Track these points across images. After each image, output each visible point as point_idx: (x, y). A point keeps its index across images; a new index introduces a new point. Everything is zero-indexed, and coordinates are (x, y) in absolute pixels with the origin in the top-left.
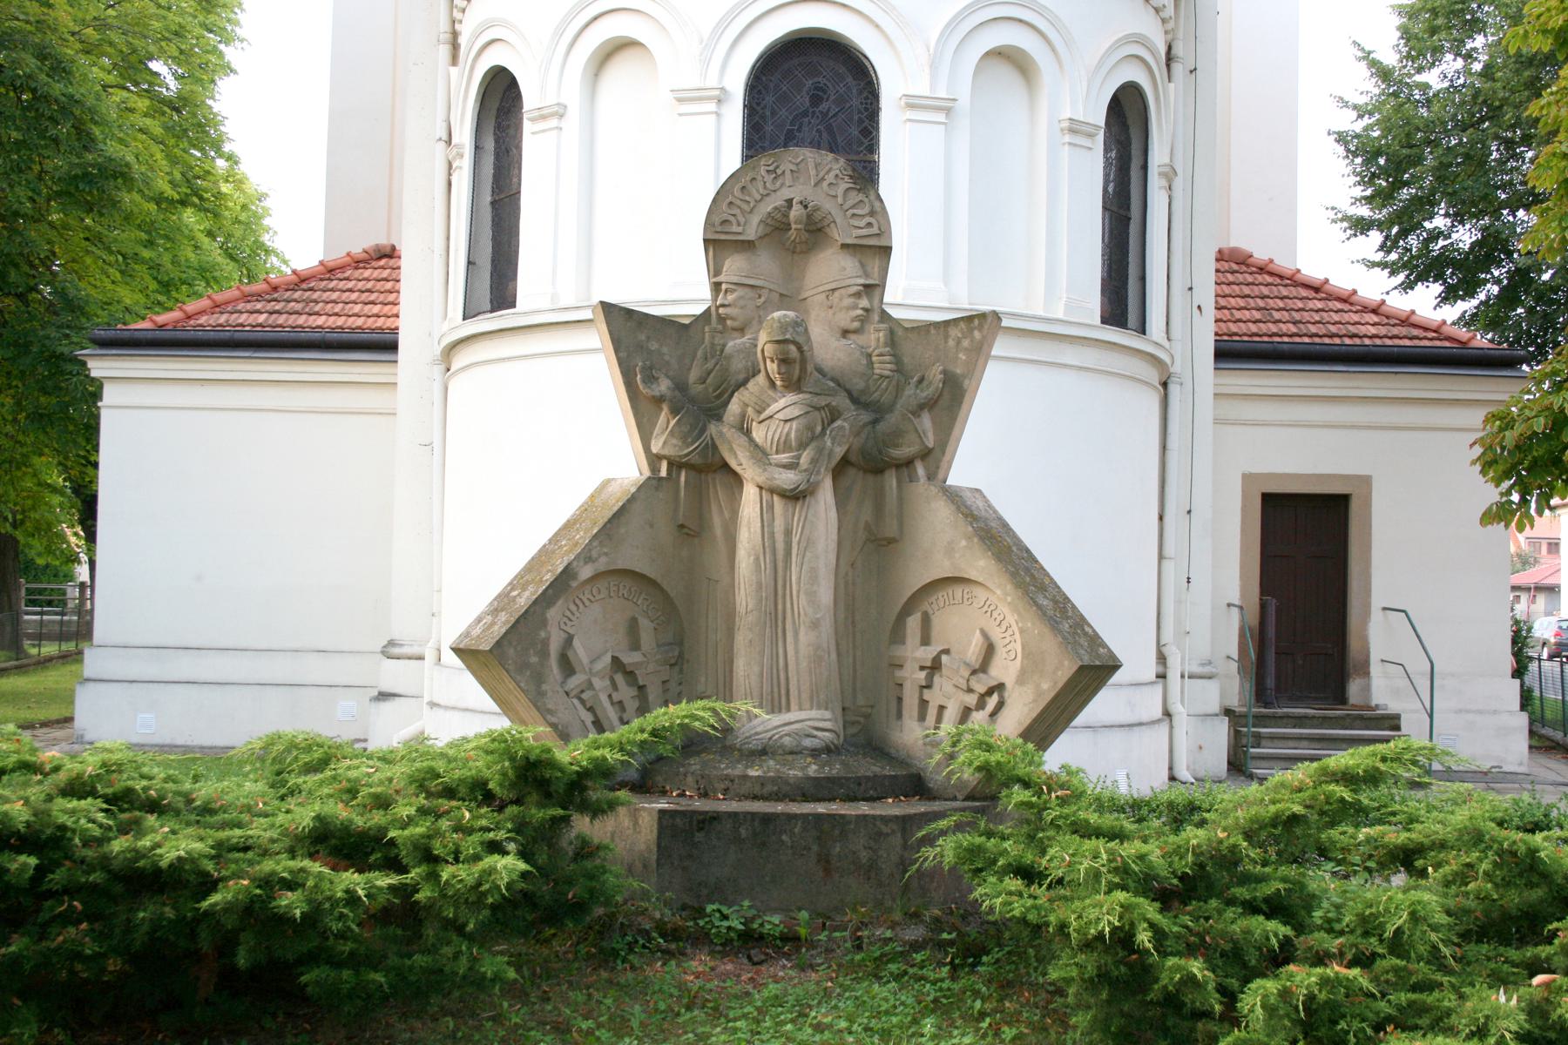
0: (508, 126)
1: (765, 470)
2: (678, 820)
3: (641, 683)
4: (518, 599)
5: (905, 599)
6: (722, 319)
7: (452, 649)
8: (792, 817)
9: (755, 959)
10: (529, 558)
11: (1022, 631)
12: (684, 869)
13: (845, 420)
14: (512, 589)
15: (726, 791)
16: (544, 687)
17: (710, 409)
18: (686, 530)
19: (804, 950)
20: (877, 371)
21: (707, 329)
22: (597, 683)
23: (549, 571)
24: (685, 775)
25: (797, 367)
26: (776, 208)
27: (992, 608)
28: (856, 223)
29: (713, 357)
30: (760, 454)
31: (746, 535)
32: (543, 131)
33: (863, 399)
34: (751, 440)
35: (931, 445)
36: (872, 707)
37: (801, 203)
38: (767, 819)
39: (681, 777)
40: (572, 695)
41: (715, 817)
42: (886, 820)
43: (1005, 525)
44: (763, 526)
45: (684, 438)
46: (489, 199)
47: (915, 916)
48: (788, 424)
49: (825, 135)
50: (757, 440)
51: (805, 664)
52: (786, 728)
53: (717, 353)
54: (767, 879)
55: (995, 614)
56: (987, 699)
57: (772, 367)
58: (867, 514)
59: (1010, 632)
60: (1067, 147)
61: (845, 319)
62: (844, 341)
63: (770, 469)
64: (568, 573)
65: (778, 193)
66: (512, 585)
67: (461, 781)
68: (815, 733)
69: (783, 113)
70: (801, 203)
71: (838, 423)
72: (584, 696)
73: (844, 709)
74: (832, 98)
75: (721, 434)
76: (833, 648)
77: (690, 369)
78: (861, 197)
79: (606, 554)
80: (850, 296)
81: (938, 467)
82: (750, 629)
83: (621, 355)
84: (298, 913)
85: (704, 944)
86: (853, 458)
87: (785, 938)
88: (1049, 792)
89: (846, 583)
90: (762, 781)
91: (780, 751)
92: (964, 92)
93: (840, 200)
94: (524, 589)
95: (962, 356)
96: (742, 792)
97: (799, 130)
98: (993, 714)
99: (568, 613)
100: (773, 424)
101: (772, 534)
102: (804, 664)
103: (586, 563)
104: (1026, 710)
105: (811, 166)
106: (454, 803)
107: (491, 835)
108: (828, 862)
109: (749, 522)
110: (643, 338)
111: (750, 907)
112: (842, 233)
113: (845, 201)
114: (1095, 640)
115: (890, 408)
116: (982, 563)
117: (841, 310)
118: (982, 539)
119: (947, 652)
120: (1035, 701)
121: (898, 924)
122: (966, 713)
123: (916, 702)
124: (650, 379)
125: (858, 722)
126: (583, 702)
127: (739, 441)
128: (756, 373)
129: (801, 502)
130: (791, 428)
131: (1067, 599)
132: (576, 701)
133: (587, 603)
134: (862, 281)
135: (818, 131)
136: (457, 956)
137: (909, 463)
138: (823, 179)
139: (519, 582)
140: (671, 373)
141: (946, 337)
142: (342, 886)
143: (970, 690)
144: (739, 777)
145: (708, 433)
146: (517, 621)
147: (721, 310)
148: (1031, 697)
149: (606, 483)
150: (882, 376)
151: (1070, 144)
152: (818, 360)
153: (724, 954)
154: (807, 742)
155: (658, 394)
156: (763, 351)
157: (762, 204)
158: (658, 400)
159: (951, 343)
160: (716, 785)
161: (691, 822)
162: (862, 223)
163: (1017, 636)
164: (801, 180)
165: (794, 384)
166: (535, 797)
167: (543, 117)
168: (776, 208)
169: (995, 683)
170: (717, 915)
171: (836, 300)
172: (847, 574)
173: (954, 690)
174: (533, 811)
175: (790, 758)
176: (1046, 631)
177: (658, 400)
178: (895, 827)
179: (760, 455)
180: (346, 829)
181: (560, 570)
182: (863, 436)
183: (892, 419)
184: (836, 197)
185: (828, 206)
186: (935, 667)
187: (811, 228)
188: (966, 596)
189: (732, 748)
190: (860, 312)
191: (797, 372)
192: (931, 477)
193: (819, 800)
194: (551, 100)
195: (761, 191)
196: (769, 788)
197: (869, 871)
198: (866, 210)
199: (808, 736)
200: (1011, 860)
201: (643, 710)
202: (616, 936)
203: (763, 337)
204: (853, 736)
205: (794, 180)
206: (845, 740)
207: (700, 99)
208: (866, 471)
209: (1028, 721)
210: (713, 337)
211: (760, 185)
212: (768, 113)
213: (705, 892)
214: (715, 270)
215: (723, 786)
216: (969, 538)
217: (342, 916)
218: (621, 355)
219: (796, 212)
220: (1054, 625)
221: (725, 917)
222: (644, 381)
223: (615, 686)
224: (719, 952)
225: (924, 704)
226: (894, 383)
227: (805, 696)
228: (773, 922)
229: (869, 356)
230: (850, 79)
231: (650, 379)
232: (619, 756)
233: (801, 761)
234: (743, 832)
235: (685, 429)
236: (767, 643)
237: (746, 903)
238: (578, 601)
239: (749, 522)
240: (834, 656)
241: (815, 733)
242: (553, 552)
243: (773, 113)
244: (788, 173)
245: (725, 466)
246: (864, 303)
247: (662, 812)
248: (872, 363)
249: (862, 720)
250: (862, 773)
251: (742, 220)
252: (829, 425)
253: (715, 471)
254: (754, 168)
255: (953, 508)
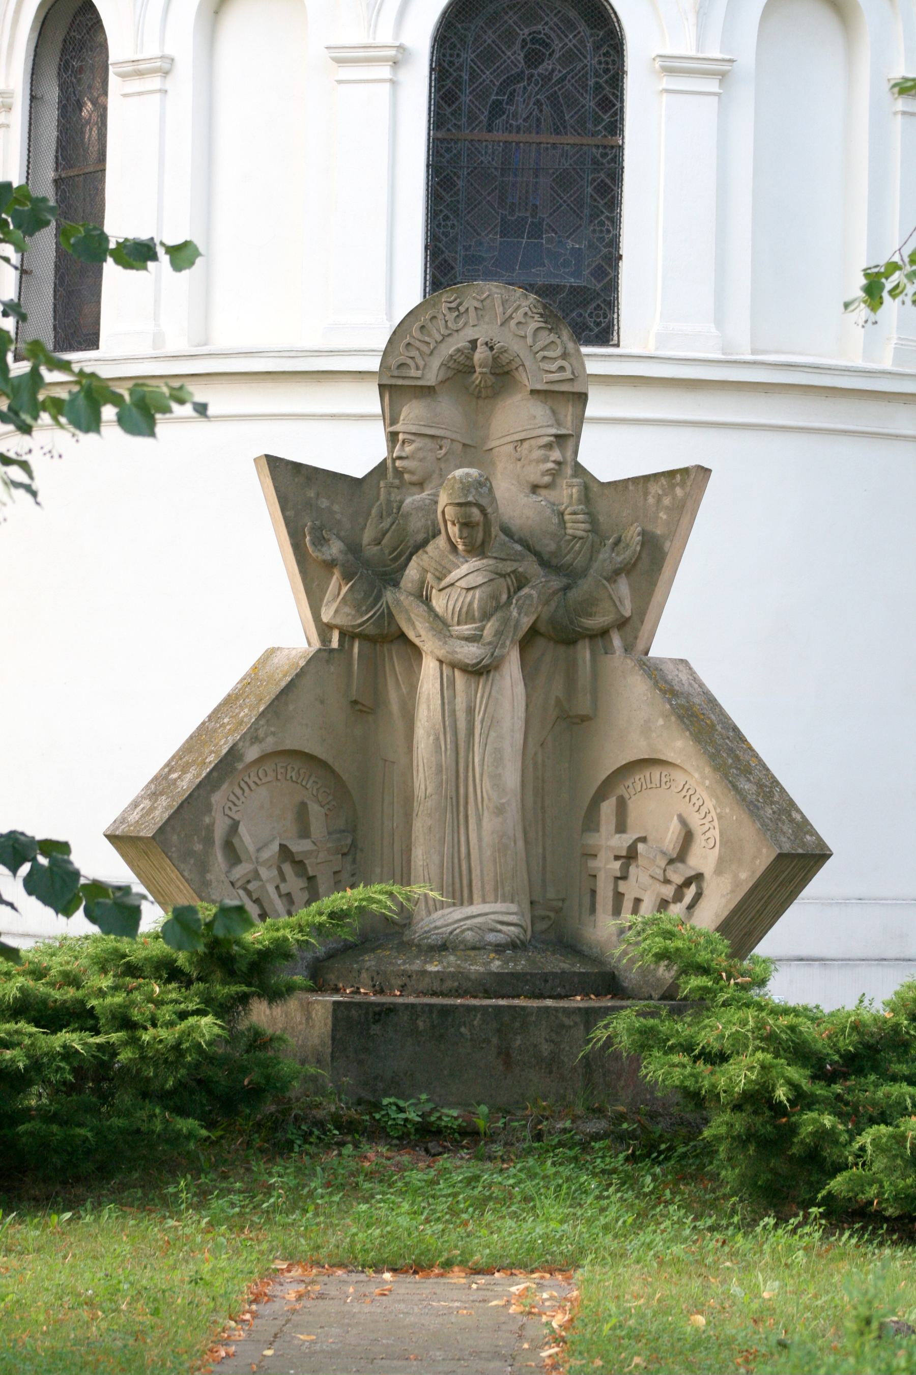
0: (81, 70)
1: (445, 643)
2: (353, 1012)
3: (311, 874)
4: (179, 783)
5: (600, 782)
6: (399, 473)
7: (107, 836)
8: (470, 1009)
9: (433, 1151)
10: (187, 736)
11: (720, 817)
12: (361, 1062)
13: (533, 587)
14: (170, 772)
15: (403, 988)
16: (209, 876)
17: (385, 573)
18: (359, 707)
19: (482, 1143)
20: (569, 531)
21: (382, 484)
22: (264, 873)
23: (211, 752)
24: (359, 972)
25: (481, 528)
26: (458, 350)
27: (691, 792)
28: (546, 366)
29: (389, 515)
30: (440, 624)
31: (426, 713)
32: (140, 94)
33: (554, 562)
34: (431, 609)
35: (627, 613)
36: (563, 900)
37: (486, 344)
38: (445, 1011)
39: (355, 974)
40: (238, 884)
41: (391, 1010)
42: (567, 1011)
43: (712, 701)
44: (443, 704)
45: (357, 607)
46: (51, 175)
47: (599, 1112)
48: (471, 593)
49: (547, 109)
50: (438, 609)
51: (489, 853)
52: (469, 922)
53: (394, 511)
54: (445, 1072)
55: (694, 799)
56: (685, 890)
57: (454, 530)
58: (558, 689)
59: (709, 818)
60: (899, 117)
61: (535, 473)
62: (534, 498)
63: (451, 641)
64: (233, 754)
65: (462, 333)
66: (170, 766)
67: (147, 959)
68: (499, 927)
69: (487, 75)
70: (486, 344)
71: (525, 591)
72: (250, 887)
73: (532, 903)
74: (557, 55)
75: (398, 602)
76: (520, 835)
77: (363, 528)
78: (552, 337)
79: (273, 734)
80: (540, 447)
81: (636, 638)
82: (430, 815)
83: (288, 513)
84: (21, 1065)
85: (380, 1138)
86: (542, 628)
87: (463, 1133)
88: (729, 979)
89: (535, 764)
90: (441, 977)
91: (462, 947)
92: (746, 57)
93: (529, 341)
94: (185, 770)
95: (663, 515)
96: (421, 988)
97: (510, 101)
98: (691, 907)
99: (233, 798)
100: (455, 593)
101: (453, 712)
102: (488, 853)
103: (252, 743)
104: (724, 901)
105: (498, 303)
106: (141, 981)
107: (182, 1006)
108: (508, 1055)
109: (428, 700)
110: (312, 495)
111: (428, 1100)
112: (529, 379)
113: (534, 342)
114: (804, 827)
115: (584, 573)
116: (679, 744)
117: (531, 461)
118: (680, 718)
119: (643, 840)
120: (732, 891)
121: (580, 1117)
122: (663, 904)
123: (610, 894)
124: (320, 541)
125: (549, 917)
126: (249, 893)
127: (417, 611)
128: (436, 534)
129: (484, 676)
130: (473, 597)
131: (775, 782)
132: (241, 892)
133: (253, 786)
134: (554, 431)
135: (538, 103)
136: (152, 1116)
137: (604, 633)
138: (511, 317)
139: (179, 762)
140: (343, 534)
141: (646, 494)
142: (60, 1042)
143: (667, 881)
144: (417, 972)
145: (383, 600)
146: (181, 806)
147: (398, 463)
148: (729, 887)
149: (271, 653)
150: (574, 537)
151: (904, 113)
152: (505, 519)
153: (400, 1148)
154: (491, 937)
155: (329, 558)
156: (443, 512)
157: (443, 345)
158: (330, 565)
159: (651, 500)
160: (393, 981)
161: (367, 1013)
162: (554, 367)
163: (716, 823)
164: (487, 319)
165: (477, 549)
166: (219, 974)
167: (140, 74)
168: (458, 350)
169: (693, 873)
170: (394, 1108)
171: (525, 452)
172: (536, 754)
173: (651, 881)
174: (218, 987)
175: (472, 953)
176: (745, 818)
177: (330, 565)
178: (578, 1019)
179: (441, 626)
180: (44, 1001)
181: (224, 751)
182: (553, 604)
183: (585, 586)
184: (525, 337)
185: (516, 347)
186: (631, 856)
187: (497, 371)
188: (664, 780)
189: (409, 945)
190: (550, 465)
191: (480, 536)
192: (628, 649)
193: (503, 997)
194: (151, 50)
195: (443, 331)
196: (450, 984)
197: (552, 1064)
198: (559, 352)
199: (492, 930)
200: (681, 1040)
201: (314, 896)
202: (291, 1128)
203: (443, 499)
204: (543, 932)
205: (479, 318)
206: (533, 936)
207: (368, 60)
208: (557, 642)
209: (726, 913)
210: (390, 494)
211: (441, 323)
212: (466, 77)
213: (381, 1085)
214: (391, 417)
215: (400, 983)
216: (666, 717)
217: (59, 1069)
218: (288, 513)
219: (480, 355)
220: (752, 808)
221: (401, 1110)
222: (313, 544)
223: (282, 877)
224: (396, 1145)
225: (619, 897)
226: (588, 544)
227: (489, 887)
228: (451, 1115)
229: (562, 514)
230: (582, 27)
231: (320, 541)
232: (299, 936)
233: (483, 957)
234: (421, 1024)
235: (360, 596)
236: (448, 831)
237: (424, 1097)
238: (243, 785)
239: (428, 700)
240: (521, 844)
241: (499, 927)
242: (215, 730)
243: (473, 76)
244: (471, 310)
245: (402, 636)
246: (556, 455)
247: (335, 1003)
248: (565, 523)
249: (552, 915)
250: (548, 969)
251: (421, 363)
252: (515, 593)
253: (392, 641)
254: (434, 306)
255: (650, 683)
